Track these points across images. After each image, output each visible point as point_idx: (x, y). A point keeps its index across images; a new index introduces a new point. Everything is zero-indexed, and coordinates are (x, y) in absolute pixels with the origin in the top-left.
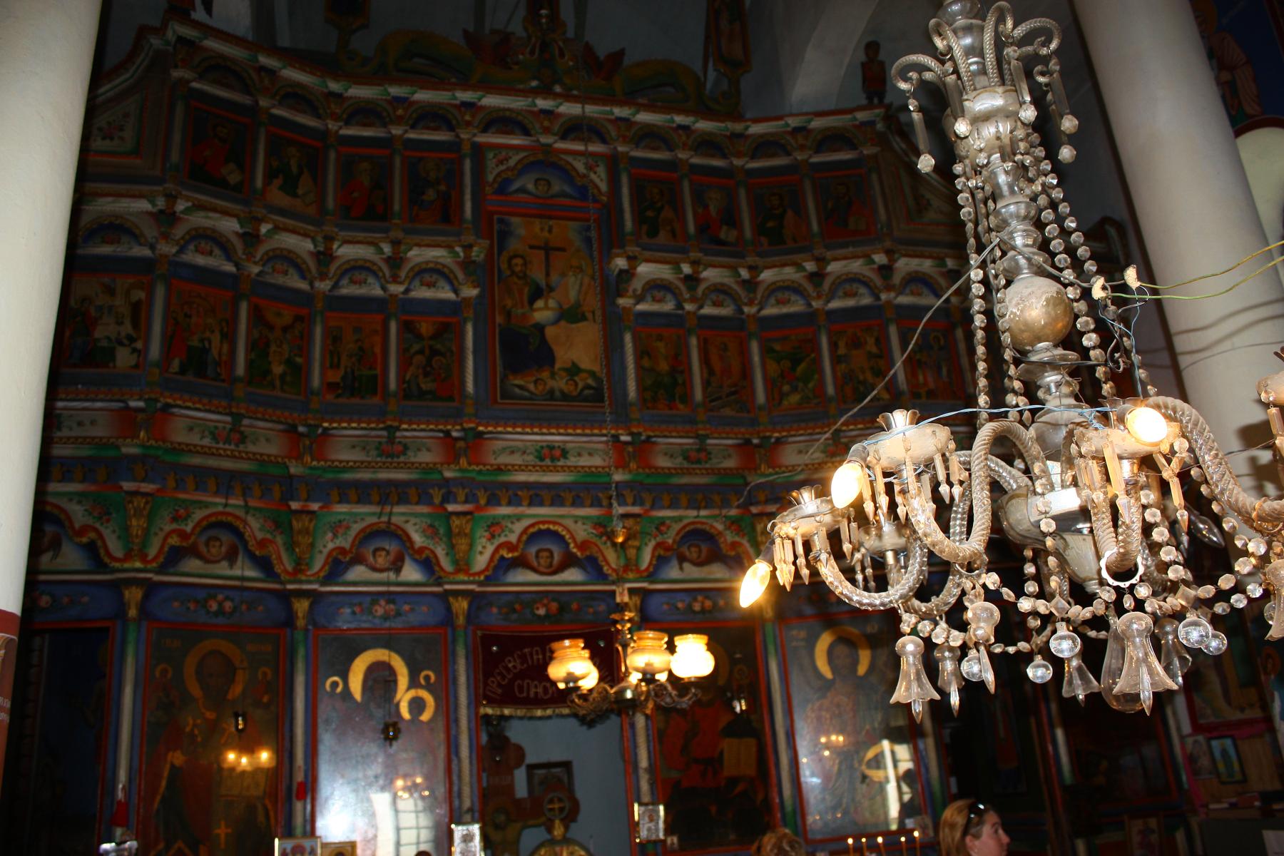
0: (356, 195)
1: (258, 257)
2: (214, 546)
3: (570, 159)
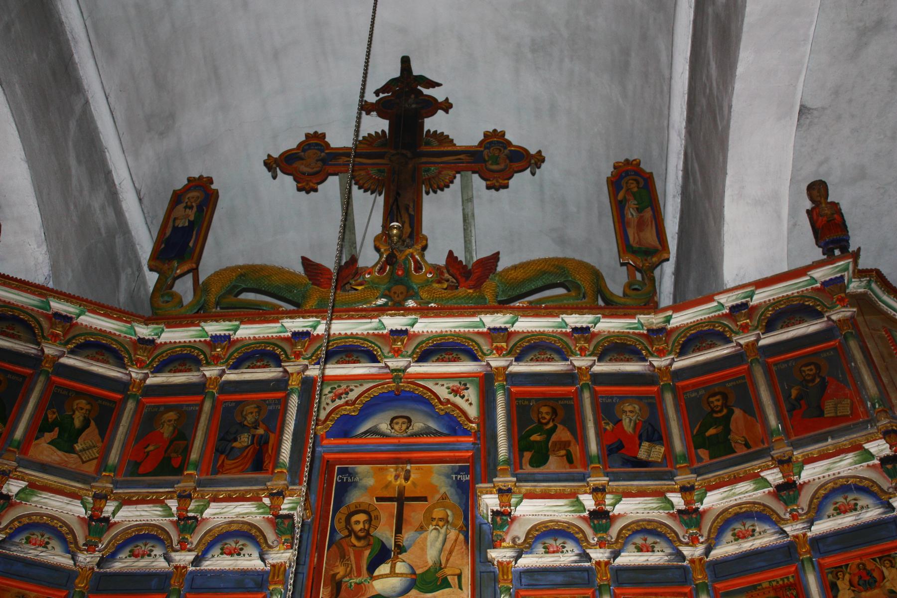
0: (151, 448)
3: (429, 384)
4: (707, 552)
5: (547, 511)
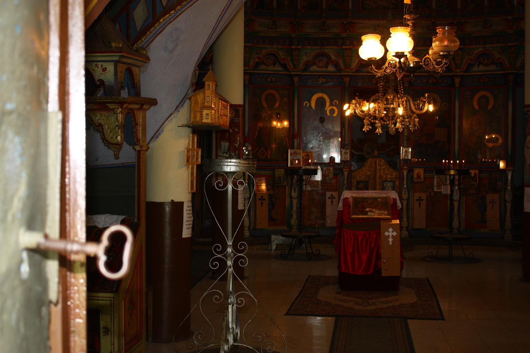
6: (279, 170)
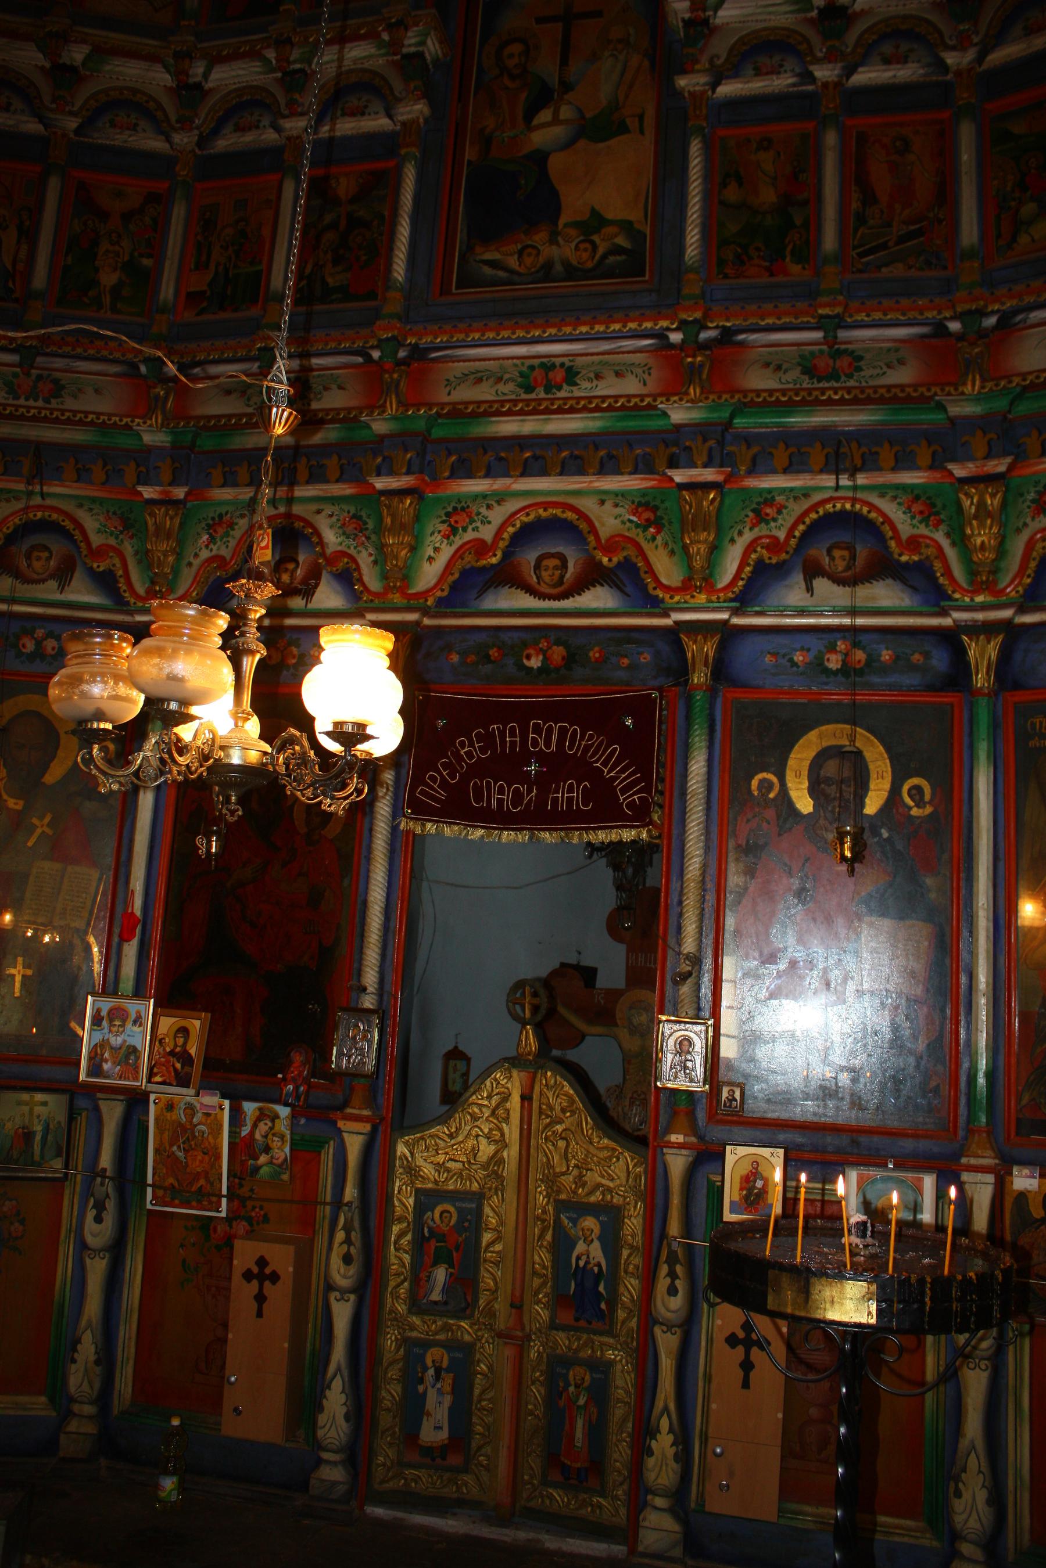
1: (79, 103)
2: (39, 559)
4: (980, 59)
5: (760, 14)
6: (25, 1096)
